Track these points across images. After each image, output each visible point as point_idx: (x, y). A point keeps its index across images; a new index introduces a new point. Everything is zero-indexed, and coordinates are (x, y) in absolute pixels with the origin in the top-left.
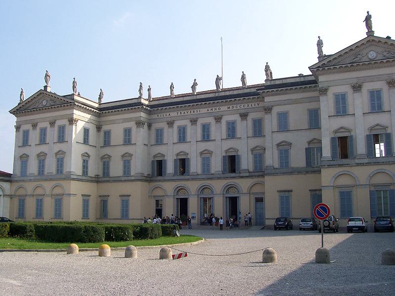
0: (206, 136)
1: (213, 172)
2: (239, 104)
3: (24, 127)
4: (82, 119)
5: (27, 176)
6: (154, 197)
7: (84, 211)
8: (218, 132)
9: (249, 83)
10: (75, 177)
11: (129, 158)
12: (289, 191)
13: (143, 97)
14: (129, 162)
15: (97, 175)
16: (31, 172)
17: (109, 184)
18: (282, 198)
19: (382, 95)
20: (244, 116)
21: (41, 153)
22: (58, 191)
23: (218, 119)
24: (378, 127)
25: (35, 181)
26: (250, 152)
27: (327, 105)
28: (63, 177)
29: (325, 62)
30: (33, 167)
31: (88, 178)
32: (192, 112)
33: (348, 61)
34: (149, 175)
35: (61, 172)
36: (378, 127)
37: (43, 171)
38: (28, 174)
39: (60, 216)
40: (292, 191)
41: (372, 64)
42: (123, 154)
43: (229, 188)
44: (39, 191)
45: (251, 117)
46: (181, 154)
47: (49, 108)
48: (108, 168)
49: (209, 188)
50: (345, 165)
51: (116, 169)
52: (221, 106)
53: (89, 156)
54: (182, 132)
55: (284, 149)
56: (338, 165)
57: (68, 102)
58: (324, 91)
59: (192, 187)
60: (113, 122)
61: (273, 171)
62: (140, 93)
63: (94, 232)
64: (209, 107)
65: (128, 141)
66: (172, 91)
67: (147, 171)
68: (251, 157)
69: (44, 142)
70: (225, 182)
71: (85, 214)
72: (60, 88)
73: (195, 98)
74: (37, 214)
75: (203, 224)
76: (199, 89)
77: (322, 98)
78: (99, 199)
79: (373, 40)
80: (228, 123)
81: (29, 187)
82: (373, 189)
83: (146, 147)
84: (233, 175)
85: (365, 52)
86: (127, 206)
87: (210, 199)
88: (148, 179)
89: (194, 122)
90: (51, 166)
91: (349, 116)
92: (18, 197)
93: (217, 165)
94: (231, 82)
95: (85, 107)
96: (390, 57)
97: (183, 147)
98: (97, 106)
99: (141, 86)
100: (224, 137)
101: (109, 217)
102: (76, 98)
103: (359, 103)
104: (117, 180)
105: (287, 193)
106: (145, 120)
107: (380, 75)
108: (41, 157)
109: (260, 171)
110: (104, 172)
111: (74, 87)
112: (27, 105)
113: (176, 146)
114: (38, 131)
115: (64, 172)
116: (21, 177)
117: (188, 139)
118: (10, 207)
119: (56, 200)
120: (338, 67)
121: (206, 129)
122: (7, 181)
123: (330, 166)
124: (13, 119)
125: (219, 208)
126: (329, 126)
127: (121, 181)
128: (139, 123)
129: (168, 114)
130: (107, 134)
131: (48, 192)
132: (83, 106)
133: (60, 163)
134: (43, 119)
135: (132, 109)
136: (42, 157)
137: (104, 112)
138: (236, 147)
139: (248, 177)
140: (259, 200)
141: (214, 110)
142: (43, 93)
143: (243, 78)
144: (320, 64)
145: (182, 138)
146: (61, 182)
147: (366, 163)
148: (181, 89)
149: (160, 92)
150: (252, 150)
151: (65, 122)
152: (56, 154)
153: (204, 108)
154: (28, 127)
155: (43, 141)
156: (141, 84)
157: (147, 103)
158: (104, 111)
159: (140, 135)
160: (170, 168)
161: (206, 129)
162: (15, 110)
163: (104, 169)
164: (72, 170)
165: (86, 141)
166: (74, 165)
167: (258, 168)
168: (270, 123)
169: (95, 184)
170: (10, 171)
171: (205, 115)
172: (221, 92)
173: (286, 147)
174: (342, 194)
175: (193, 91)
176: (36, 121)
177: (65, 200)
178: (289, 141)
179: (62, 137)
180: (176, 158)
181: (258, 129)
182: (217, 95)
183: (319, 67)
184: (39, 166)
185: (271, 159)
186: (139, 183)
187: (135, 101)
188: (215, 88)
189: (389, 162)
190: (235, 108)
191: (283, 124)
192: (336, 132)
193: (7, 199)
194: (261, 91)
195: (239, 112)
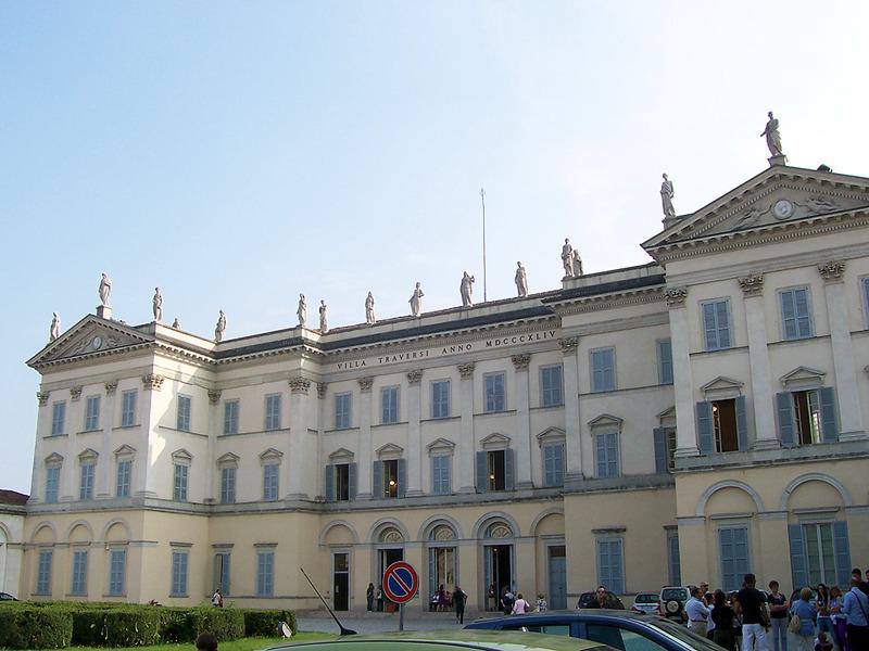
0: (441, 411)
1: (455, 489)
2: (511, 334)
3: (55, 397)
4: (173, 379)
5: (57, 502)
6: (332, 546)
7: (175, 578)
8: (467, 398)
9: (533, 288)
10: (156, 504)
11: (275, 461)
12: (617, 531)
13: (306, 325)
14: (275, 468)
15: (210, 500)
16: (66, 494)
17: (232, 519)
18: (176, 555)
19: (809, 298)
20: (521, 361)
21: (86, 451)
22: (118, 534)
23: (467, 370)
24: (802, 375)
25: (73, 512)
26: (536, 445)
27: (685, 328)
28: (93, 505)
29: (678, 230)
30: (70, 485)
31: (186, 507)
32: (411, 355)
33: (729, 226)
34: (320, 497)
35: (126, 493)
36: (802, 375)
37: (89, 491)
38: (59, 497)
39: (119, 590)
40: (625, 530)
41: (784, 230)
42: (262, 451)
43: (491, 525)
44: (79, 536)
45: (536, 363)
46: (388, 449)
47: (104, 354)
48: (232, 483)
49: (506, 525)
50: (729, 465)
51: (249, 487)
52: (473, 340)
53: (189, 458)
54: (391, 401)
55: (607, 431)
56: (713, 466)
57: (141, 341)
58: (678, 297)
59: (412, 523)
60: (243, 382)
61: (583, 485)
62: (301, 318)
63: (43, 624)
64: (447, 344)
65: (273, 424)
66: (369, 310)
67: (314, 488)
68: (538, 453)
69: (94, 427)
70: (480, 513)
71: (179, 588)
72: (127, 311)
73: (416, 324)
74: (75, 584)
75: (433, 607)
76: (425, 306)
77: (674, 314)
78: (213, 553)
79: (782, 176)
81: (61, 526)
82: (795, 521)
83: (313, 436)
84: (499, 495)
85: (766, 204)
86: (270, 568)
87: (450, 550)
88: (319, 507)
89: (415, 377)
90: (106, 482)
91: (737, 352)
92: (38, 549)
93: (464, 474)
94: (497, 288)
95: (180, 349)
96: (822, 212)
97: (391, 435)
98: (210, 347)
99: (301, 302)
100: (480, 409)
101: (231, 594)
102: (159, 330)
103: (757, 319)
104: (250, 510)
105: (615, 534)
106: (312, 376)
107: (829, 250)
108: (88, 459)
109: (557, 485)
110: (224, 494)
111: (156, 307)
112: (63, 349)
113: (376, 432)
114: (82, 403)
115: (132, 492)
116: (222, 504)
117: (403, 417)
118: (22, 571)
119: (114, 553)
120: (705, 240)
121: (440, 393)
122: (16, 513)
123: (694, 470)
124: (35, 378)
125: (470, 577)
126: (694, 376)
127: (257, 512)
128: (297, 384)
129: (360, 362)
130: (232, 409)
131: (97, 537)
132: (174, 348)
133: (125, 472)
134: (91, 375)
135: (281, 352)
136: (89, 460)
137: (224, 360)
138: (506, 431)
139: (529, 499)
140: (558, 552)
141: (457, 349)
142: (93, 324)
143: (519, 278)
144: (666, 237)
145: (390, 416)
146: (127, 516)
147: (776, 461)
148: (393, 307)
149: (346, 315)
150: (541, 438)
151: (135, 383)
152: (118, 453)
153: (436, 346)
154: (63, 395)
155: (91, 426)
156: (370, 295)
157: (316, 338)
158: (225, 358)
159: (302, 410)
160: (364, 482)
161: (440, 393)
162: (38, 359)
163: (224, 485)
164: (147, 489)
165: (183, 424)
166: (155, 477)
167: (554, 478)
168: (577, 373)
169: (204, 519)
170: (24, 489)
171: (437, 362)
172: (472, 309)
173: (611, 429)
174: (725, 535)
175: (413, 309)
176: (836, 257)
177: (132, 552)
178: (739, 379)
179: (131, 417)
180: (377, 460)
181: (552, 393)
182: (464, 316)
183: (664, 242)
184: (83, 480)
185: (580, 458)
186: (297, 516)
187: (290, 335)
188: (460, 303)
189: (830, 456)
190: (502, 345)
191: (604, 381)
192: (707, 389)
193: (17, 553)
194: (553, 304)
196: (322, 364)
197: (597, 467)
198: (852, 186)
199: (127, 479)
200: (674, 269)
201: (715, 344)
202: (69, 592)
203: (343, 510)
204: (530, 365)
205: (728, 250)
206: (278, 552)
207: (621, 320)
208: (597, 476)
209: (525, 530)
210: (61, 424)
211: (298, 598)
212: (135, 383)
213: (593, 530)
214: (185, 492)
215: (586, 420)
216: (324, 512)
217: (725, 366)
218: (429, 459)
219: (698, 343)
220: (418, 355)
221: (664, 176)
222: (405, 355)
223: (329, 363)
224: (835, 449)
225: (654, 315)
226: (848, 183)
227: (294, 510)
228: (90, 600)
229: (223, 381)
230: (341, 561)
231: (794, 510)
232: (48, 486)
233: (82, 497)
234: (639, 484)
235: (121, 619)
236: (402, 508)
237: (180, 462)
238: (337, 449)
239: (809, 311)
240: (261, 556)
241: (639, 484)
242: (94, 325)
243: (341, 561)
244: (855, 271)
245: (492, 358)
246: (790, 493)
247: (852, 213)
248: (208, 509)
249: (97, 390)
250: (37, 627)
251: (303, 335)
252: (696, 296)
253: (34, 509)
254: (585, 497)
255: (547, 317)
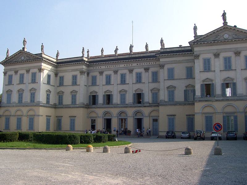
0: (123, 82)
1: (127, 103)
3: (9, 73)
4: (47, 68)
7: (47, 125)
8: (131, 78)
11: (75, 94)
12: (174, 115)
13: (85, 56)
14: (75, 96)
15: (55, 104)
16: (14, 101)
18: (47, 119)
20: (147, 70)
22: (31, 113)
23: (131, 71)
24: (228, 79)
25: (16, 106)
26: (150, 92)
27: (199, 65)
31: (50, 106)
32: (115, 66)
34: (87, 104)
35: (33, 101)
36: (228, 79)
37: (21, 101)
40: (175, 115)
41: (226, 42)
44: (19, 113)
48: (62, 100)
49: (141, 113)
51: (67, 100)
53: (50, 92)
54: (108, 78)
55: (171, 90)
57: (38, 58)
58: (197, 57)
60: (66, 71)
61: (165, 103)
65: (74, 83)
67: (86, 102)
70: (134, 109)
72: (33, 49)
73: (116, 58)
78: (56, 118)
79: (227, 28)
80: (137, 74)
81: (13, 110)
82: (225, 115)
83: (86, 87)
86: (74, 123)
88: (87, 107)
89: (116, 72)
91: (212, 72)
92: (5, 117)
93: (129, 99)
94: (139, 48)
98: (55, 61)
101: (62, 130)
102: (43, 56)
103: (217, 64)
104: (68, 107)
109: (156, 103)
111: (42, 49)
112: (12, 59)
113: (104, 87)
115: (36, 101)
116: (58, 105)
117: (112, 83)
121: (123, 77)
123: (200, 101)
125: (131, 125)
126: (200, 78)
127: (70, 107)
128: (82, 72)
129: (99, 67)
130: (62, 78)
133: (33, 96)
134: (22, 68)
136: (21, 92)
140: (155, 120)
142: (22, 52)
143: (147, 46)
145: (108, 82)
146: (34, 108)
149: (95, 53)
150: (151, 90)
151: (36, 70)
158: (60, 64)
159: (82, 80)
160: (100, 100)
161: (123, 77)
162: (3, 62)
163: (59, 100)
164: (40, 101)
165: (49, 83)
166: (42, 97)
168: (163, 74)
169: (53, 109)
171: (122, 68)
172: (133, 54)
174: (206, 117)
176: (239, 50)
177: (36, 119)
179: (34, 79)
181: (155, 78)
182: (130, 56)
183: (195, 42)
185: (163, 96)
186: (82, 109)
187: (80, 59)
189: (235, 99)
190: (141, 65)
191: (171, 76)
194: (158, 55)
195: (144, 67)
196: (88, 67)
197: (168, 99)
198: (245, 32)
199: (34, 97)
200: (196, 49)
201: (206, 70)
202: (16, 129)
203: (94, 108)
204: (149, 71)
205: (211, 45)
206: (76, 119)
207: (177, 61)
208: (168, 101)
209: (147, 115)
210: (11, 81)
211: (83, 131)
212: (36, 70)
213: (167, 115)
214: (49, 101)
215: (166, 87)
216: (89, 108)
217: (209, 75)
218: (119, 95)
219: (202, 69)
220: (117, 66)
221: (195, 24)
222: (113, 66)
223: (90, 67)
224: (236, 98)
225: (185, 60)
226: (244, 31)
227: (81, 107)
228: (23, 131)
229: (59, 70)
230: (93, 121)
231: (224, 112)
232: (8, 98)
233: (19, 102)
234: (180, 104)
235: (86, 137)
236: (112, 107)
237: (48, 93)
238: (92, 91)
239: (231, 63)
240: (71, 120)
241: (180, 104)
242: (22, 53)
243: (93, 121)
244: (243, 54)
245: (138, 69)
246: (224, 108)
247: (244, 39)
248: (55, 106)
249: (24, 72)
250: (73, 139)
251: (84, 59)
252: (202, 57)
253: (3, 105)
254: (165, 106)
255: (155, 58)
